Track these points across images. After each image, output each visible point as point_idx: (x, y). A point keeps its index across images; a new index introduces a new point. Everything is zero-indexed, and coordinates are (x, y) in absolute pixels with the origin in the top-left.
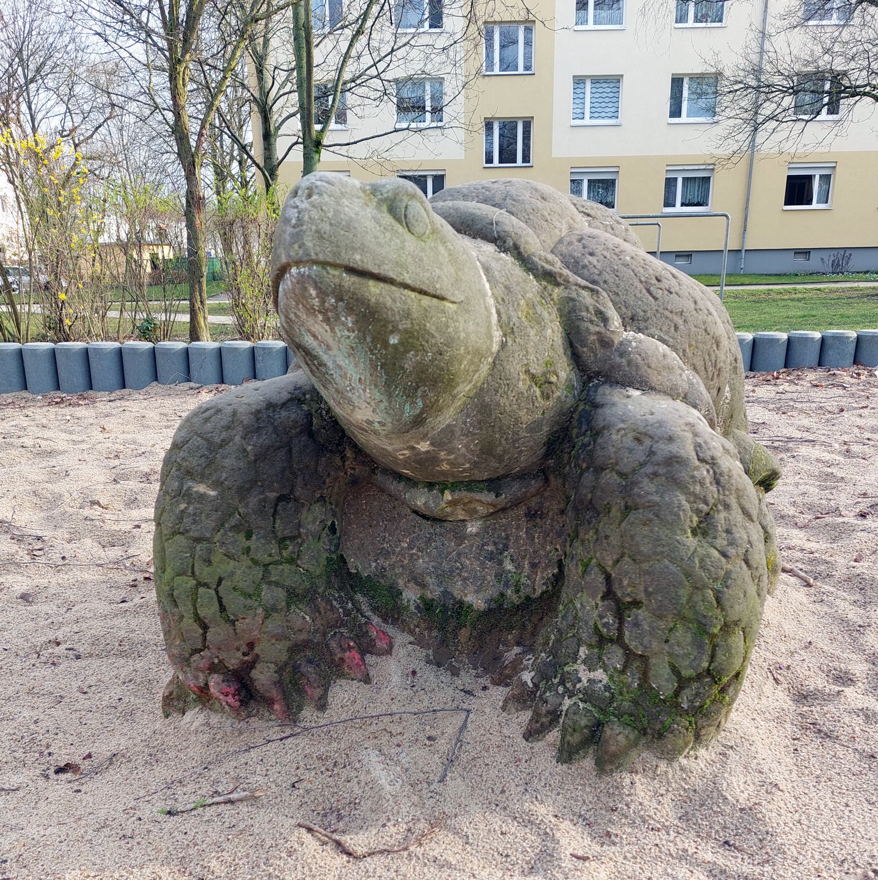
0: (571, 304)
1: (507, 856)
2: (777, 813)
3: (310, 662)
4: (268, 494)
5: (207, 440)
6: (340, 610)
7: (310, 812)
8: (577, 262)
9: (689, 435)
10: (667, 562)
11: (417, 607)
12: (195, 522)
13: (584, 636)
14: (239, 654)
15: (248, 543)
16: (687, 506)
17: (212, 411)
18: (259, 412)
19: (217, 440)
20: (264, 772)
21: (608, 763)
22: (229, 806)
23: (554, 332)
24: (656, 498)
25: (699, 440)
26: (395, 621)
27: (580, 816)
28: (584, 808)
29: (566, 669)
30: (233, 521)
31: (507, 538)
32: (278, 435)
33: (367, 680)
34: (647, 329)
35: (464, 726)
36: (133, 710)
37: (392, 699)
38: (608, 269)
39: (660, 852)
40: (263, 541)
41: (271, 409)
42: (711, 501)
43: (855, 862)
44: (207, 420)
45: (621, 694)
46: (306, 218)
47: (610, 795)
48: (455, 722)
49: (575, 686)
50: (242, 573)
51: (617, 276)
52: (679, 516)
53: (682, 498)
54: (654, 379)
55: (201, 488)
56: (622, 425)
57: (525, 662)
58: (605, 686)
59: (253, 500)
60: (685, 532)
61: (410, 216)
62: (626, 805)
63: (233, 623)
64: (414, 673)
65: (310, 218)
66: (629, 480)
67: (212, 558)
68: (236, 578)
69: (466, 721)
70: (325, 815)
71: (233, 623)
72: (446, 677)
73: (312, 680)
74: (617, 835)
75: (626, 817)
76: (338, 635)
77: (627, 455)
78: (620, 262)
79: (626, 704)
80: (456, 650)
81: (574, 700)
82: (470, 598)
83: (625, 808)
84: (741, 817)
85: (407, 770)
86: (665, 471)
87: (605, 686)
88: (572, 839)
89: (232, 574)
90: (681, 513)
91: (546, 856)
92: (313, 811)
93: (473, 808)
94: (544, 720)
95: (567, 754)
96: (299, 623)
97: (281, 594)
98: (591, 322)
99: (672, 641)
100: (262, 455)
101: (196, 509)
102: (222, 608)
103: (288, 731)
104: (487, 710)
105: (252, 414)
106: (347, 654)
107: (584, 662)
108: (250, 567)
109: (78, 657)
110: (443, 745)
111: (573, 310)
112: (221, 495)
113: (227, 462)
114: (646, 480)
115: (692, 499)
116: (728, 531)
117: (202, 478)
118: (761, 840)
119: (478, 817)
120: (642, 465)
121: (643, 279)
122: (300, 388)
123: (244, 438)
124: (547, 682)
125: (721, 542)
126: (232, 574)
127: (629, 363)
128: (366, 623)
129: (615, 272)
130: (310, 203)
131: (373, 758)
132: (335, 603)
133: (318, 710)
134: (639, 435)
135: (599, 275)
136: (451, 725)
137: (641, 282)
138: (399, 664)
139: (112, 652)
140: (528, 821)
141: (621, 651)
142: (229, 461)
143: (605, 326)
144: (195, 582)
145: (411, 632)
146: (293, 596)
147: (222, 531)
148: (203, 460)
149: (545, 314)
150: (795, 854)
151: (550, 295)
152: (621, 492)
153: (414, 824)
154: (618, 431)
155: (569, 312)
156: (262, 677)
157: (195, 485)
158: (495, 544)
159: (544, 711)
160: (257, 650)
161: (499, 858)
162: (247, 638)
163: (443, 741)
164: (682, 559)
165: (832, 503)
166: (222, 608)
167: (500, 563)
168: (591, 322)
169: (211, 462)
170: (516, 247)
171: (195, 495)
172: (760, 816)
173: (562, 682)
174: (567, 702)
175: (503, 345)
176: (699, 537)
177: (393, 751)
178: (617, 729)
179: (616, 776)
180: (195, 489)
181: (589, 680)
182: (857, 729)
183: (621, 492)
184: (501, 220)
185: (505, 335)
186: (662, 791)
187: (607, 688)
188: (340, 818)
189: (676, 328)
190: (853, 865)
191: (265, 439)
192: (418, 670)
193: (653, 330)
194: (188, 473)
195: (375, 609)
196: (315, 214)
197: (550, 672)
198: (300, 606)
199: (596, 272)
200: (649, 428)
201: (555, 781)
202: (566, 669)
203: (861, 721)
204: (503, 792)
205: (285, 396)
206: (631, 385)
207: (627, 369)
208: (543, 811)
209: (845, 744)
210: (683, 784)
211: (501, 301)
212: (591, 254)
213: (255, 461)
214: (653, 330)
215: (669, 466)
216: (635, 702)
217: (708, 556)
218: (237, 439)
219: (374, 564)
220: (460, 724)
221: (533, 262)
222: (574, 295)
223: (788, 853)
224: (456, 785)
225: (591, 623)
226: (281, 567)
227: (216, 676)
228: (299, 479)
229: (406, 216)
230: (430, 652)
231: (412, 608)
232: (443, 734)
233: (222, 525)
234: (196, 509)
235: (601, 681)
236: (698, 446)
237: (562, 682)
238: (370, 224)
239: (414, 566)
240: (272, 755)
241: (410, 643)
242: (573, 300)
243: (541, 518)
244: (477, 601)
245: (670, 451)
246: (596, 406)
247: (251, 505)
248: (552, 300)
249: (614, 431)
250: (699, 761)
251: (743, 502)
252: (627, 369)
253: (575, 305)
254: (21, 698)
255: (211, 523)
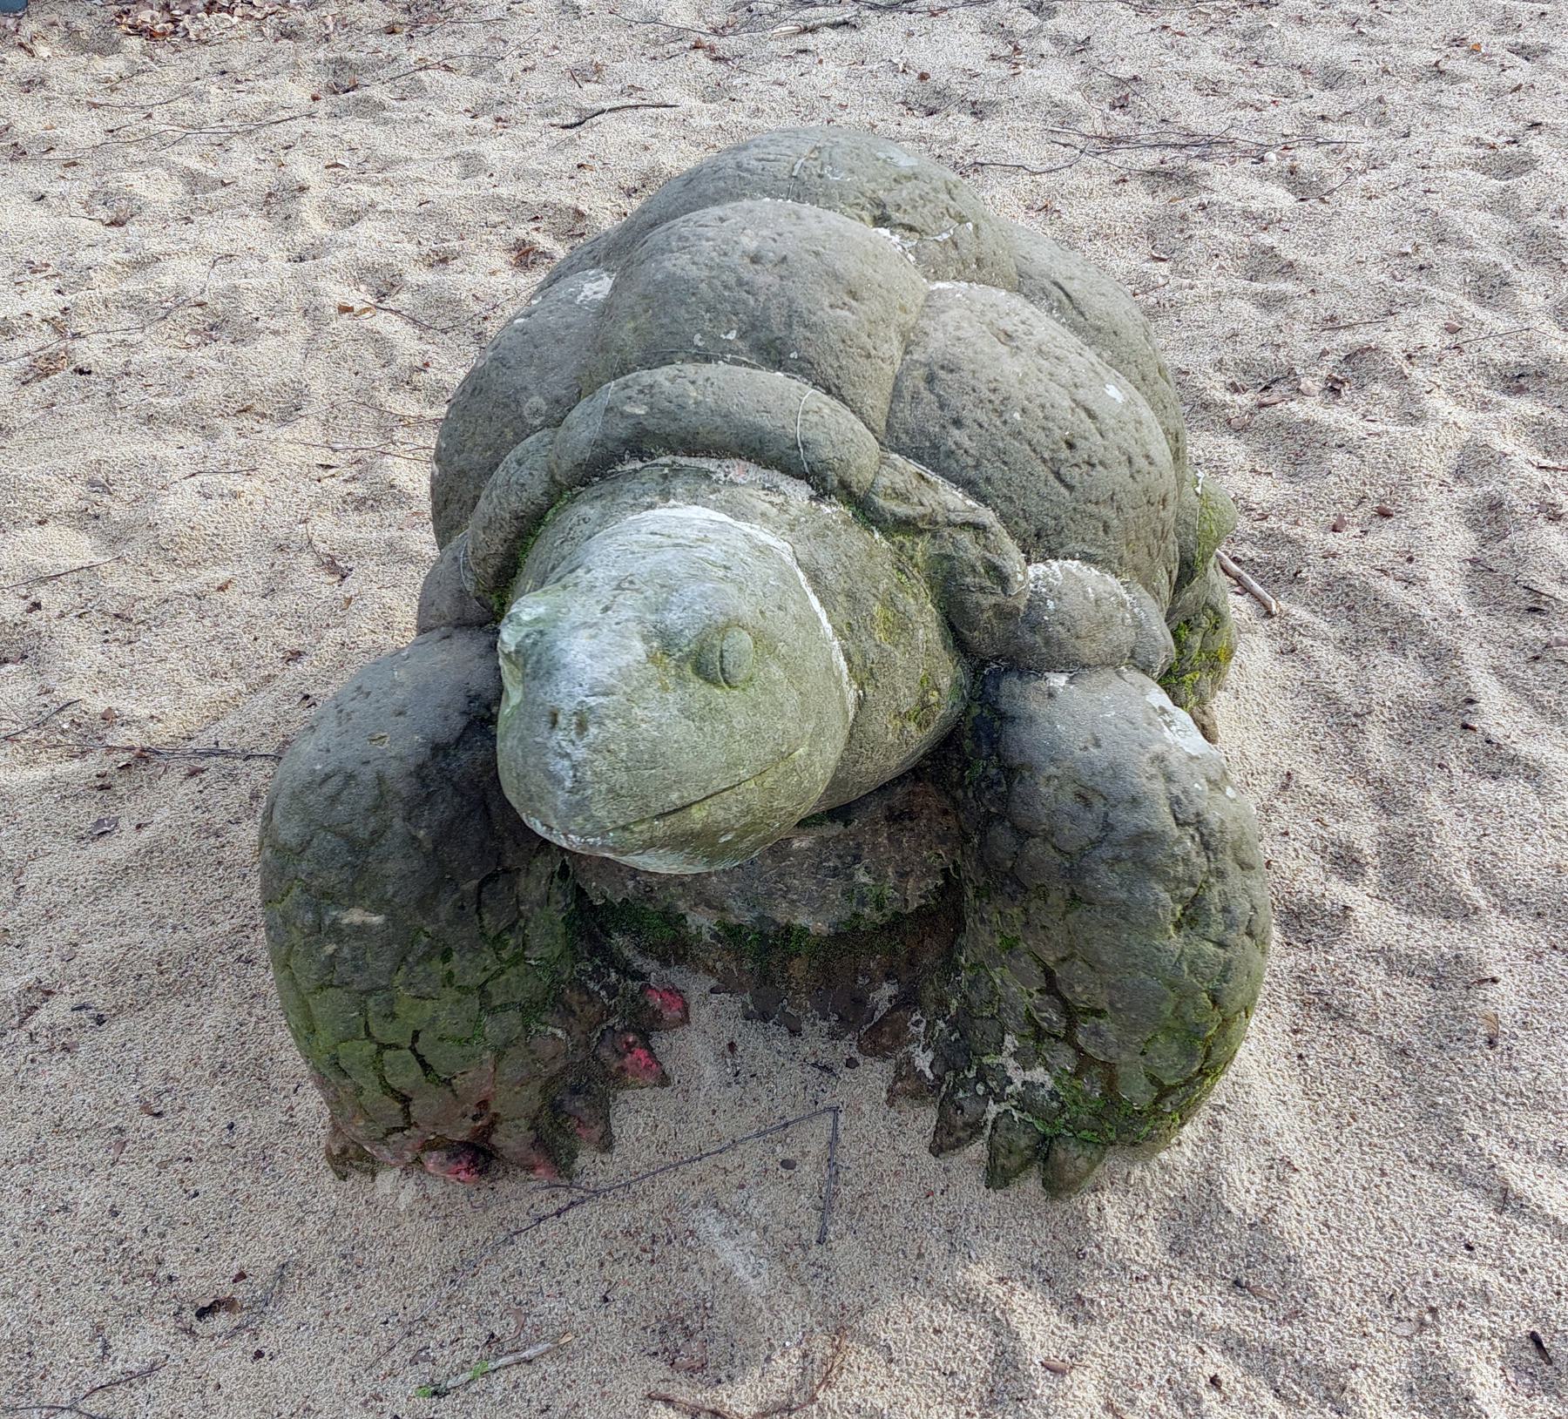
0: (946, 564)
1: (952, 1373)
2: (1298, 1223)
3: (575, 1091)
4: (465, 887)
5: (343, 835)
6: (603, 993)
7: (641, 1333)
8: (935, 447)
9: (1159, 785)
10: (1143, 975)
11: (715, 936)
12: (357, 969)
13: (1011, 1023)
14: (468, 1122)
15: (448, 966)
16: (1165, 896)
17: (336, 781)
18: (421, 767)
19: (363, 834)
20: (555, 1288)
21: (1057, 1187)
22: (526, 1369)
23: (927, 628)
24: (1124, 895)
25: (1176, 790)
26: (681, 960)
27: (1033, 1267)
28: (1036, 1252)
29: (985, 1060)
30: (419, 950)
31: (859, 846)
32: (463, 795)
33: (664, 1080)
34: (1062, 545)
35: (834, 1141)
36: (264, 1148)
37: (714, 1112)
38: (989, 453)
39: (1155, 1321)
40: (470, 956)
41: (441, 754)
42: (1200, 878)
43: (1406, 1298)
44: (334, 799)
45: (1075, 1103)
46: (589, 776)
47: (1071, 1231)
48: (817, 1132)
49: (1003, 1089)
50: (445, 1014)
51: (1005, 463)
52: (1157, 915)
53: (1158, 888)
54: (1087, 650)
55: (355, 916)
56: (1052, 770)
57: (913, 1029)
58: (1050, 1093)
59: (445, 910)
60: (1166, 930)
61: (729, 668)
62: (1097, 1246)
63: (448, 1082)
64: (732, 1046)
65: (595, 773)
66: (1075, 869)
67: (396, 1009)
68: (441, 1024)
69: (835, 1128)
70: (663, 1332)
71: (448, 1082)
72: (783, 1043)
73: (585, 1119)
74: (1092, 1301)
75: (1100, 1267)
76: (609, 1035)
77: (1068, 824)
78: (1006, 429)
79: (1085, 1117)
80: (788, 988)
81: (1004, 1106)
82: (802, 920)
83: (1096, 1251)
84: (1252, 1238)
85: (765, 1229)
86: (1130, 852)
87: (1050, 1093)
88: (1037, 1325)
89: (434, 1019)
90: (1160, 911)
91: (1005, 1373)
92: (644, 1328)
93: (885, 1291)
94: (961, 1134)
95: (997, 1176)
96: (549, 1049)
97: (513, 1018)
98: (982, 589)
99: (1151, 1054)
100: (445, 835)
101: (354, 949)
102: (426, 1067)
103: (564, 1198)
104: (866, 1108)
105: (411, 774)
106: (629, 1058)
107: (1014, 1055)
108: (459, 1001)
109: (100, 1020)
110: (808, 1173)
111: (950, 576)
112: (392, 917)
113: (391, 867)
114: (1103, 868)
115: (1173, 886)
116: (1225, 910)
117: (354, 899)
118: (1282, 1273)
119: (895, 1308)
120: (1096, 843)
121: (1046, 455)
122: (477, 697)
123: (407, 819)
124: (957, 1075)
125: (1215, 930)
126: (434, 1019)
127: (1047, 642)
128: (642, 990)
129: (1000, 453)
130: (588, 746)
131: (711, 1226)
132: (591, 985)
133: (603, 1152)
134: (1083, 791)
135: (976, 467)
136: (812, 1141)
137: (1044, 461)
138: (705, 1032)
139: (154, 991)
140: (966, 1301)
141: (1072, 1051)
142: (394, 866)
143: (1004, 591)
144: (375, 1047)
145: (710, 971)
146: (530, 1010)
147: (404, 969)
148: (347, 871)
149: (913, 606)
150: (1330, 1295)
151: (911, 558)
152: (1063, 876)
153: (808, 1342)
154: (1049, 779)
155: (945, 579)
156: (510, 1143)
157: (343, 914)
158: (840, 857)
159: (960, 1123)
160: (493, 1109)
161: (942, 1380)
162: (476, 1098)
163: (807, 1168)
164: (1164, 970)
165: (1282, 352)
166: (426, 1067)
167: (850, 877)
168: (982, 589)
169: (359, 871)
170: (844, 485)
171: (348, 931)
172: (1276, 1232)
173: (981, 1078)
174: (993, 1109)
175: (861, 703)
176: (1186, 929)
177: (735, 1198)
178: (1075, 1151)
179: (1075, 1200)
180: (346, 921)
181: (1024, 1083)
182: (1379, 993)
183: (1063, 876)
184: (810, 435)
185: (861, 686)
186: (1141, 1210)
187: (1054, 1095)
188: (689, 1334)
189: (1106, 528)
190: (1404, 1303)
191: (443, 811)
192: (737, 1040)
193: (1073, 546)
194: (325, 895)
195: (643, 952)
196: (601, 765)
197: (959, 1060)
198: (543, 1018)
199: (971, 462)
200: (1098, 779)
201: (990, 1220)
202: (985, 1060)
203: (1383, 976)
204: (920, 1256)
205: (458, 722)
206: (1053, 668)
207: (1044, 650)
208: (981, 1276)
209: (1365, 1027)
210: (1167, 1190)
211: (847, 631)
212: (957, 423)
213: (435, 849)
214: (1073, 546)
215: (1136, 844)
216: (1098, 1116)
217: (1200, 955)
218: (398, 823)
219: (631, 884)
220: (827, 1135)
221: (877, 509)
222: (949, 549)
223: (1322, 1294)
224: (846, 1251)
225: (1022, 1009)
226: (503, 977)
227: (435, 1154)
228: (508, 843)
229: (723, 670)
230: (748, 998)
231: (707, 937)
232: (804, 1154)
233: (404, 959)
234: (354, 949)
235: (1043, 1085)
236: (1175, 802)
237: (981, 1078)
238: (681, 730)
239: (704, 886)
240: (559, 1251)
241: (712, 991)
242: (948, 557)
243: (911, 819)
244: (815, 923)
245: (1136, 825)
246: (1005, 718)
247: (442, 916)
248: (916, 565)
249: (1042, 780)
250: (1185, 1146)
251: (1242, 855)
252: (1044, 650)
253: (952, 568)
254: (50, 1147)
255: (384, 964)
